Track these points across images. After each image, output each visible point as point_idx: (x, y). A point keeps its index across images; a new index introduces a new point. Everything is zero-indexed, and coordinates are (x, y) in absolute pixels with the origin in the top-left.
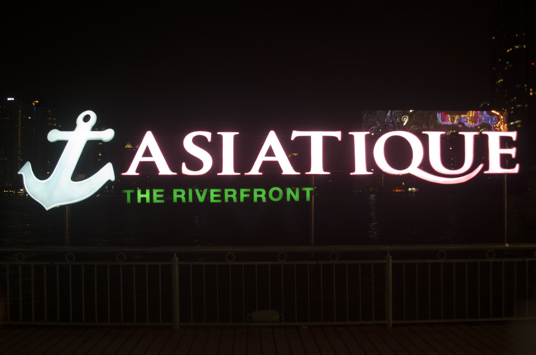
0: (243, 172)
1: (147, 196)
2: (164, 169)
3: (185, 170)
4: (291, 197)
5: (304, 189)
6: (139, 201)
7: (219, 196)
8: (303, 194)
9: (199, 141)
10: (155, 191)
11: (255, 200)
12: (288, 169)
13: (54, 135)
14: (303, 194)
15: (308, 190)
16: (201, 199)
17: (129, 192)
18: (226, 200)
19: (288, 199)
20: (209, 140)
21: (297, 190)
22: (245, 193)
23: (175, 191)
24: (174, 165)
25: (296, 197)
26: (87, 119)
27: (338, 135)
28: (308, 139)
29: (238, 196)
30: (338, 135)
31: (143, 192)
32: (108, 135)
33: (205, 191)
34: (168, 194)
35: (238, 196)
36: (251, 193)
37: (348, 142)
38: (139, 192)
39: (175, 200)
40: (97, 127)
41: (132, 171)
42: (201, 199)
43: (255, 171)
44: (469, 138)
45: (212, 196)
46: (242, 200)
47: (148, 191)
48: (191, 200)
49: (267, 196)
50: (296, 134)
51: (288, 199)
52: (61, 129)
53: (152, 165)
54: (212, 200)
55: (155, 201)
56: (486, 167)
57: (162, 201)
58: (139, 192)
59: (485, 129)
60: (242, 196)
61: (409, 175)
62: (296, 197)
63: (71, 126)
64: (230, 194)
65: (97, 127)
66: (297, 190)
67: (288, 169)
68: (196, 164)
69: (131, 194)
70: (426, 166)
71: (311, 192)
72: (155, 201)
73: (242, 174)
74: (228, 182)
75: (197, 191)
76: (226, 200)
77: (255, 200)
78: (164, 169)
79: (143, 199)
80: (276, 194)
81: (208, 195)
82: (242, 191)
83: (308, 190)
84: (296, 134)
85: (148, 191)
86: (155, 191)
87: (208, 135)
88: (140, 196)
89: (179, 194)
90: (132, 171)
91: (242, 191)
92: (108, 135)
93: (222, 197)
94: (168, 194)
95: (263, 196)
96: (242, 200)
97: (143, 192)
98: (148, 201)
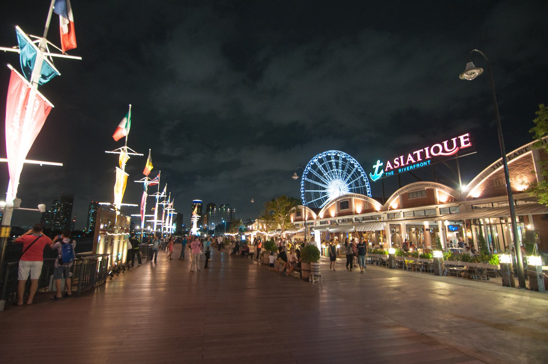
4: (425, 162)
5: (428, 161)
8: (428, 163)
9: (397, 160)
14: (428, 163)
15: (429, 161)
16: (405, 170)
21: (426, 162)
24: (393, 167)
27: (422, 150)
37: (424, 151)
43: (407, 163)
46: (414, 168)
49: (420, 165)
51: (424, 165)
52: (158, 208)
57: (469, 145)
59: (461, 74)
62: (426, 164)
63: (376, 164)
65: (380, 163)
66: (426, 162)
67: (413, 161)
68: (396, 165)
70: (444, 151)
71: (430, 162)
74: (403, 167)
79: (390, 174)
80: (421, 165)
81: (406, 169)
82: (414, 166)
95: (419, 166)
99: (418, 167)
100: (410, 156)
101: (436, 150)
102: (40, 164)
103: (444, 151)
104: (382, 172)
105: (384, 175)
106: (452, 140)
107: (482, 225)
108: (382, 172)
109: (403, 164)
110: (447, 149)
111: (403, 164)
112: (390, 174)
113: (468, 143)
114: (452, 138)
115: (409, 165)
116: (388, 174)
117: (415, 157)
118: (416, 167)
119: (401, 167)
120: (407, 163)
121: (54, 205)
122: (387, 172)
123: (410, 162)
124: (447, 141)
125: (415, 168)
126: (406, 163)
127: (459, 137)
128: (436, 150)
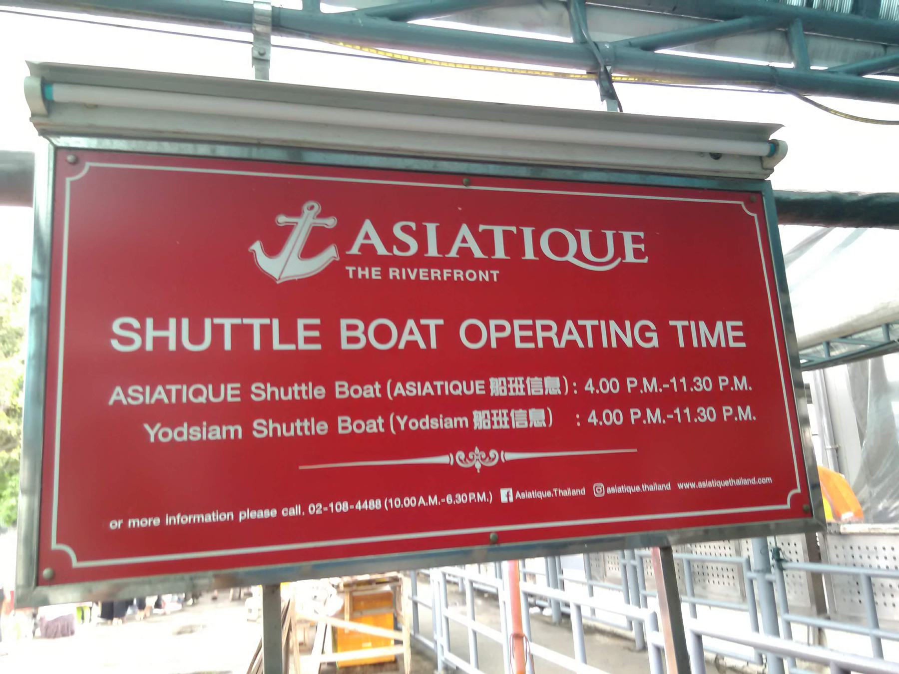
0: (444, 254)
1: (367, 272)
2: (381, 250)
3: (396, 252)
6: (360, 276)
7: (427, 274)
8: (491, 276)
9: (405, 229)
10: (373, 269)
11: (456, 279)
12: (478, 253)
13: (282, 220)
14: (491, 276)
15: (495, 273)
16: (413, 277)
17: (351, 269)
18: (433, 278)
19: (481, 279)
20: (515, 232)
21: (487, 272)
22: (447, 273)
23: (391, 270)
25: (487, 279)
26: (312, 208)
27: (514, 229)
28: (492, 231)
29: (442, 275)
30: (514, 229)
31: (363, 269)
32: (330, 222)
33: (415, 271)
34: (385, 273)
35: (442, 275)
36: (452, 273)
37: (521, 233)
38: (359, 269)
39: (391, 277)
40: (320, 216)
41: (355, 250)
42: (413, 277)
43: (453, 253)
44: (609, 234)
45: (421, 274)
46: (445, 278)
47: (367, 269)
48: (404, 277)
49: (464, 276)
50: (482, 227)
51: (481, 279)
53: (372, 247)
54: (421, 278)
55: (374, 277)
56: (624, 257)
58: (359, 269)
60: (445, 276)
61: (567, 262)
62: (487, 279)
64: (435, 273)
66: (487, 272)
67: (478, 253)
68: (404, 247)
69: (353, 271)
70: (579, 255)
71: (497, 274)
72: (374, 277)
73: (490, 257)
75: (409, 271)
76: (433, 278)
77: (456, 279)
78: (381, 250)
79: (363, 276)
80: (471, 275)
82: (445, 271)
83: (495, 273)
84: (482, 227)
85: (367, 269)
86: (373, 269)
87: (413, 225)
88: (360, 272)
89: (394, 272)
90: (355, 250)
91: (445, 271)
92: (330, 222)
93: (429, 276)
94: (385, 273)
96: (445, 278)
97: (363, 269)
98: (367, 277)
99: (459, 278)
100: (465, 231)
101: (558, 243)
102: (654, 347)
103: (579, 255)
104: (330, 254)
105: (334, 269)
106: (360, 253)
107: (447, 334)
108: (330, 254)
109: (433, 251)
110: (587, 252)
111: (433, 251)
112: (363, 276)
113: (643, 258)
114: (359, 255)
115: (452, 264)
116: (355, 273)
117: (486, 241)
118: (450, 279)
119: (420, 260)
120: (453, 253)
121: (441, 496)
122: (354, 260)
123: (465, 252)
124: (347, 253)
125: (448, 277)
126: (449, 251)
127: (441, 256)
128: (558, 243)
